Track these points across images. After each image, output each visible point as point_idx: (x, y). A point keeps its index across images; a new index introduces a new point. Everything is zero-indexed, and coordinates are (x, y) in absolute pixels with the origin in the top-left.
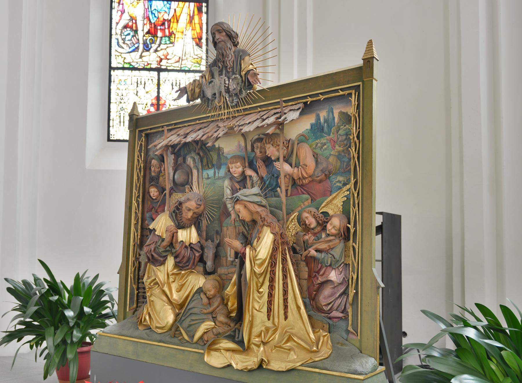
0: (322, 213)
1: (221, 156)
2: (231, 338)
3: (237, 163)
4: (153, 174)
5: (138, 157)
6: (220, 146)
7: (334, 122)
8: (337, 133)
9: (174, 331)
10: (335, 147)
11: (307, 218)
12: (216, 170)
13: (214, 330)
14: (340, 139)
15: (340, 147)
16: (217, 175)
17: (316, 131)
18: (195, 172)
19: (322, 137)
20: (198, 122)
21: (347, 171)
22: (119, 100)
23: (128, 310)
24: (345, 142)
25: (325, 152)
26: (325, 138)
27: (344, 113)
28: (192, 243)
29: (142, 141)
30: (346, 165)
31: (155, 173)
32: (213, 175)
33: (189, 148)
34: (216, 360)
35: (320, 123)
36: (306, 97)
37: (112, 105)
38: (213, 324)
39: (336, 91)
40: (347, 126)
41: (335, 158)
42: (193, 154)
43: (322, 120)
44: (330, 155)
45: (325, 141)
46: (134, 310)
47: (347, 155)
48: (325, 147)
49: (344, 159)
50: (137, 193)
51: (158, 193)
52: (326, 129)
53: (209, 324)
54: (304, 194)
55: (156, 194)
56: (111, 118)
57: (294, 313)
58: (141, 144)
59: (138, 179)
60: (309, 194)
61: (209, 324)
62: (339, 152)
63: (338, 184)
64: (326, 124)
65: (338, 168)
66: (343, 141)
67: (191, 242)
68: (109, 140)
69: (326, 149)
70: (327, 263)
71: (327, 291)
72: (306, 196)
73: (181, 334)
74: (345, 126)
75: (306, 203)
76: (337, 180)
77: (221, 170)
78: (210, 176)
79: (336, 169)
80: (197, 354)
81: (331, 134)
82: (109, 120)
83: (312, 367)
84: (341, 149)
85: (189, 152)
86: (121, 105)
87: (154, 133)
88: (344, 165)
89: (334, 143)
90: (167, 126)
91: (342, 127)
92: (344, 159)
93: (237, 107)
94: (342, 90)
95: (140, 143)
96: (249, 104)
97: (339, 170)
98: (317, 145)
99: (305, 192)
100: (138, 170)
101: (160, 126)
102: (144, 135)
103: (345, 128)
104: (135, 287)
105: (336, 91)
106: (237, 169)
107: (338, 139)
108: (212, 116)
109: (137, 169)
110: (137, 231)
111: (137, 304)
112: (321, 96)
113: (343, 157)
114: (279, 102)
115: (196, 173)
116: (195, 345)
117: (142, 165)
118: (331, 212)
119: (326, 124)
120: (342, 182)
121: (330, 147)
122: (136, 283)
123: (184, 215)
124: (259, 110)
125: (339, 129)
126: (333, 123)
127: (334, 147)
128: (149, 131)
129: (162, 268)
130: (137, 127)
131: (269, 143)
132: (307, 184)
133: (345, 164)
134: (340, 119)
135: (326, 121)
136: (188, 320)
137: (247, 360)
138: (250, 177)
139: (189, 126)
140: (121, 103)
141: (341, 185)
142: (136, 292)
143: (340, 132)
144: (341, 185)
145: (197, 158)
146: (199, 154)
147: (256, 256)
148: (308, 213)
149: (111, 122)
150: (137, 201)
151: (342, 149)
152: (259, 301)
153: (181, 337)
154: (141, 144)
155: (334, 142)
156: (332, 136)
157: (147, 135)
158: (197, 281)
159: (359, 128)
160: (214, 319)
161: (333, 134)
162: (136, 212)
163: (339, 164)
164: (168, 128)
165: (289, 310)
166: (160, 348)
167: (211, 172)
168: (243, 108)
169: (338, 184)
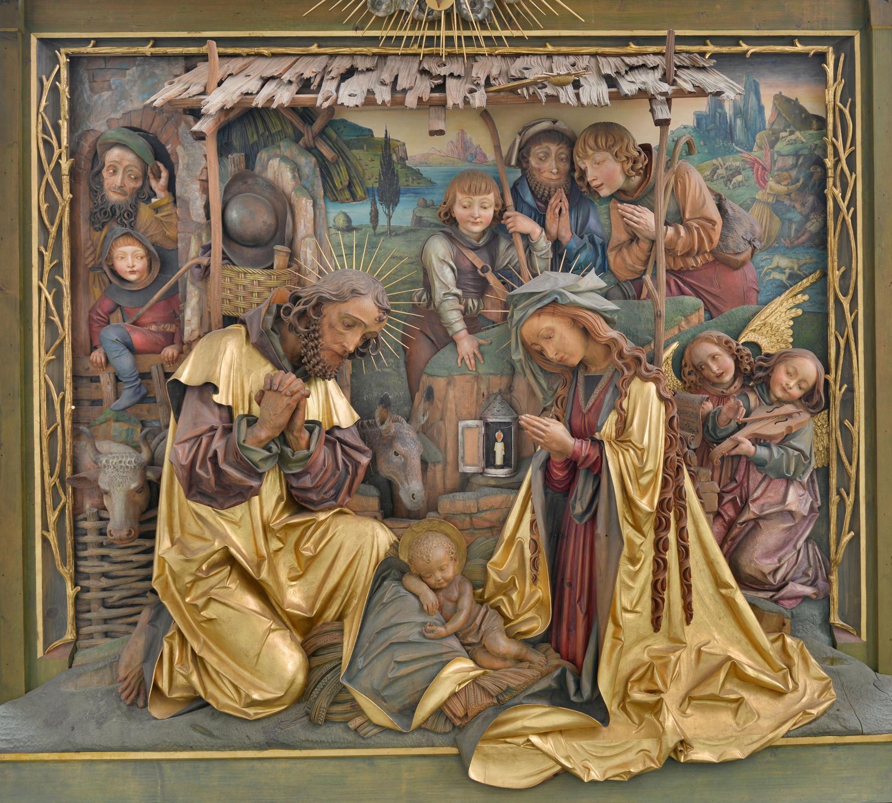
0: (744, 344)
1: (398, 168)
2: (557, 697)
3: (489, 193)
4: (114, 198)
5: (45, 130)
6: (392, 136)
7: (763, 119)
8: (772, 147)
9: (320, 699)
10: (765, 182)
11: (713, 357)
12: (381, 209)
13: (487, 683)
14: (779, 164)
15: (778, 183)
16: (383, 220)
17: (712, 134)
18: (305, 208)
19: (731, 152)
20: (314, 49)
21: (798, 246)
24: (794, 173)
25: (739, 191)
26: (738, 156)
27: (788, 100)
28: (338, 428)
29: (58, 77)
30: (797, 231)
31: (124, 194)
32: (367, 220)
33: (266, 128)
35: (723, 116)
36: (702, 40)
38: (471, 664)
39: (790, 41)
40: (798, 133)
41: (767, 211)
42: (287, 148)
43: (728, 108)
44: (754, 200)
45: (738, 164)
46: (69, 650)
47: (798, 206)
48: (739, 178)
49: (789, 215)
50: (47, 255)
51: (145, 261)
52: (739, 133)
53: (458, 670)
54: (682, 293)
55: (140, 264)
57: (707, 601)
58: (54, 90)
59: (53, 209)
60: (698, 295)
61: (458, 670)
62: (777, 195)
63: (776, 275)
64: (739, 122)
65: (774, 233)
66: (787, 170)
67: (336, 421)
69: (740, 185)
70: (788, 471)
71: (770, 536)
72: (691, 300)
73: (358, 710)
74: (792, 133)
75: (694, 319)
76: (774, 265)
77: (399, 209)
78: (354, 224)
79: (769, 237)
80: (426, 762)
81: (755, 148)
83: (815, 735)
84: (782, 188)
85: (269, 141)
87: (107, 58)
88: (790, 228)
89: (762, 174)
90: (219, 41)
91: (783, 134)
92: (789, 215)
93: (431, 28)
94: (804, 40)
95: (47, 85)
96: (526, 27)
97: (777, 240)
98: (714, 172)
99: (687, 289)
100: (49, 177)
101: (147, 40)
102: (63, 60)
103: (793, 137)
104: (67, 572)
105: (790, 41)
106: (477, 211)
107: (774, 162)
108: (389, 38)
109: (42, 172)
110: (60, 388)
111: (77, 629)
112: (744, 47)
113: (789, 210)
114: (664, 38)
115: (310, 209)
116: (416, 736)
117: (65, 165)
118: (768, 345)
119: (739, 122)
120: (787, 271)
121: (753, 181)
122: (70, 560)
123: (327, 339)
124: (550, 48)
125: (777, 140)
126: (759, 120)
127: (762, 182)
128: (89, 49)
129: (239, 511)
131: (608, 149)
132: (696, 269)
133: (794, 227)
134: (779, 114)
135: (739, 112)
136: (378, 667)
138: (526, 237)
139: (274, 55)
141: (783, 278)
142: (70, 591)
143: (779, 146)
144: (783, 278)
145: (307, 163)
146: (310, 150)
147: (644, 467)
148: (718, 344)
150: (54, 284)
151: (785, 188)
152: (631, 584)
153: (358, 721)
154: (54, 90)
155: (764, 168)
156: (756, 153)
157: (74, 62)
158: (359, 539)
159: (853, 143)
160: (472, 650)
161: (760, 148)
162: (49, 323)
163: (777, 225)
164: (222, 50)
165: (694, 597)
166: (267, 764)
167: (360, 212)
168: (508, 33)
169: (776, 275)
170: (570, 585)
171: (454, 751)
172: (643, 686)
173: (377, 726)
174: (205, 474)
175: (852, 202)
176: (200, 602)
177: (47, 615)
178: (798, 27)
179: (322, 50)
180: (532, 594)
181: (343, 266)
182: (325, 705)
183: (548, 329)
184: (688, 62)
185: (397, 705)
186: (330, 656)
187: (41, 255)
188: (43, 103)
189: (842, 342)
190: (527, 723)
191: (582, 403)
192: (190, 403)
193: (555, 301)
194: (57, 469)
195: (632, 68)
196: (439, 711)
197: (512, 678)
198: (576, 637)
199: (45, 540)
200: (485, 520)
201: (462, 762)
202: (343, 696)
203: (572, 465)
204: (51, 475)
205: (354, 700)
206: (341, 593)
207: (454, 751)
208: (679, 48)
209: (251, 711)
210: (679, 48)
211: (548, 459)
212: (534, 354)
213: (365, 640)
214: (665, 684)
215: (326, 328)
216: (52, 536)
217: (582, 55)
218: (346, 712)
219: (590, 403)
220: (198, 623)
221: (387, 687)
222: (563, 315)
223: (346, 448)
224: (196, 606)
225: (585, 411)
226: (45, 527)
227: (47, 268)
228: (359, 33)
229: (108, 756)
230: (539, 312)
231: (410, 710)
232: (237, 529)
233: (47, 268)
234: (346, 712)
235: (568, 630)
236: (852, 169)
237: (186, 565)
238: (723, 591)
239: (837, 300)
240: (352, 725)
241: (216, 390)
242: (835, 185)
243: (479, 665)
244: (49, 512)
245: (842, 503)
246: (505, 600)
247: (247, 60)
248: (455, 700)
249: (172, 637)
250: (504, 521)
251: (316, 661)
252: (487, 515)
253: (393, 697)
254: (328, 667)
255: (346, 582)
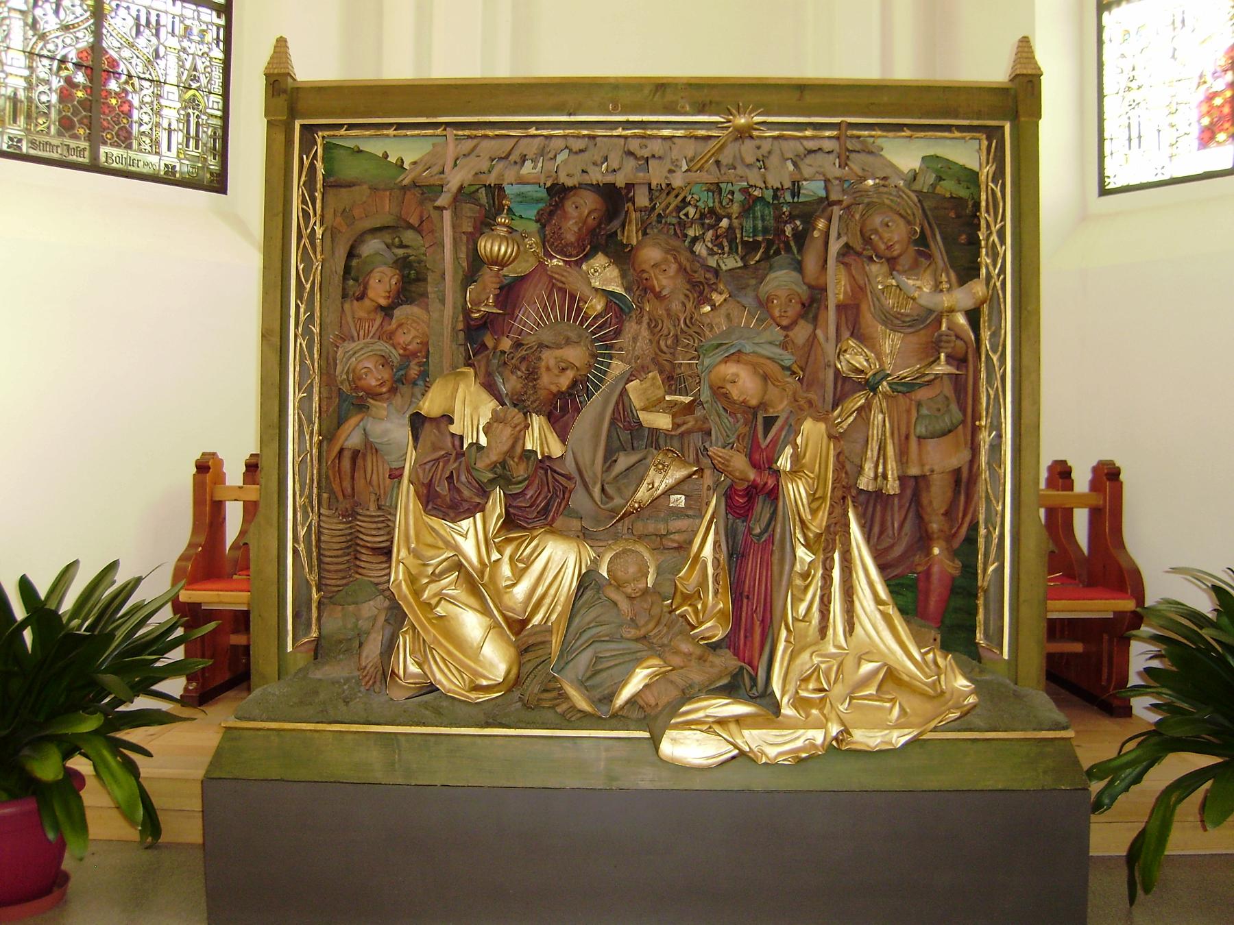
5: (304, 202)
13: (674, 676)
20: (533, 131)
22: (1124, 83)
23: (290, 649)
28: (549, 457)
34: (690, 747)
37: (1107, 102)
56: (1106, 135)
58: (312, 167)
68: (1104, 191)
80: (622, 743)
82: (1101, 140)
86: (1130, 96)
95: (306, 163)
100: (305, 240)
101: (391, 125)
104: (313, 578)
110: (311, 422)
130: (293, 113)
137: (787, 738)
140: (1129, 89)
149: (1107, 144)
162: (302, 363)
166: (487, 740)
170: (748, 597)
171: (646, 735)
172: (811, 686)
173: (580, 711)
174: (442, 489)
175: (1003, 270)
176: (433, 602)
177: (296, 616)
178: (956, 117)
179: (539, 132)
180: (715, 605)
181: (555, 317)
182: (536, 691)
183: (733, 374)
184: (858, 147)
185: (597, 694)
186: (540, 652)
187: (297, 307)
188: (303, 179)
189: (992, 393)
190: (710, 711)
191: (761, 440)
192: (428, 432)
193: (739, 351)
194: (307, 491)
195: (810, 152)
196: (631, 701)
197: (697, 676)
198: (752, 642)
199: (295, 551)
200: (673, 541)
201: (655, 741)
202: (552, 685)
203: (752, 492)
204: (301, 496)
205: (561, 688)
206: (547, 601)
207: (646, 735)
208: (849, 133)
209: (473, 695)
210: (849, 133)
211: (731, 487)
212: (719, 393)
213: (569, 637)
214: (828, 683)
215: (543, 370)
216: (301, 548)
217: (766, 137)
218: (556, 699)
219: (768, 440)
220: (429, 620)
221: (590, 678)
222: (746, 363)
223: (557, 476)
224: (429, 604)
225: (763, 446)
226: (295, 539)
227: (302, 318)
228: (573, 118)
229: (354, 728)
230: (727, 360)
231: (610, 698)
232: (468, 537)
233: (302, 318)
234: (556, 699)
235: (746, 637)
236: (1003, 242)
237: (422, 568)
238: (881, 608)
239: (987, 355)
240: (559, 710)
241: (451, 421)
242: (987, 254)
243: (667, 663)
244: (299, 528)
245: (988, 536)
246: (690, 609)
247: (475, 141)
248: (647, 692)
249: (406, 632)
250: (691, 542)
251: (528, 656)
252: (676, 537)
253: (594, 687)
254: (539, 661)
255: (552, 591)
